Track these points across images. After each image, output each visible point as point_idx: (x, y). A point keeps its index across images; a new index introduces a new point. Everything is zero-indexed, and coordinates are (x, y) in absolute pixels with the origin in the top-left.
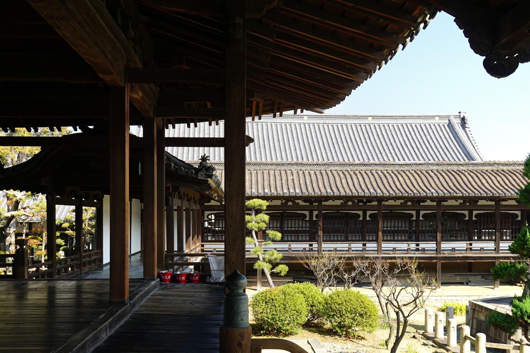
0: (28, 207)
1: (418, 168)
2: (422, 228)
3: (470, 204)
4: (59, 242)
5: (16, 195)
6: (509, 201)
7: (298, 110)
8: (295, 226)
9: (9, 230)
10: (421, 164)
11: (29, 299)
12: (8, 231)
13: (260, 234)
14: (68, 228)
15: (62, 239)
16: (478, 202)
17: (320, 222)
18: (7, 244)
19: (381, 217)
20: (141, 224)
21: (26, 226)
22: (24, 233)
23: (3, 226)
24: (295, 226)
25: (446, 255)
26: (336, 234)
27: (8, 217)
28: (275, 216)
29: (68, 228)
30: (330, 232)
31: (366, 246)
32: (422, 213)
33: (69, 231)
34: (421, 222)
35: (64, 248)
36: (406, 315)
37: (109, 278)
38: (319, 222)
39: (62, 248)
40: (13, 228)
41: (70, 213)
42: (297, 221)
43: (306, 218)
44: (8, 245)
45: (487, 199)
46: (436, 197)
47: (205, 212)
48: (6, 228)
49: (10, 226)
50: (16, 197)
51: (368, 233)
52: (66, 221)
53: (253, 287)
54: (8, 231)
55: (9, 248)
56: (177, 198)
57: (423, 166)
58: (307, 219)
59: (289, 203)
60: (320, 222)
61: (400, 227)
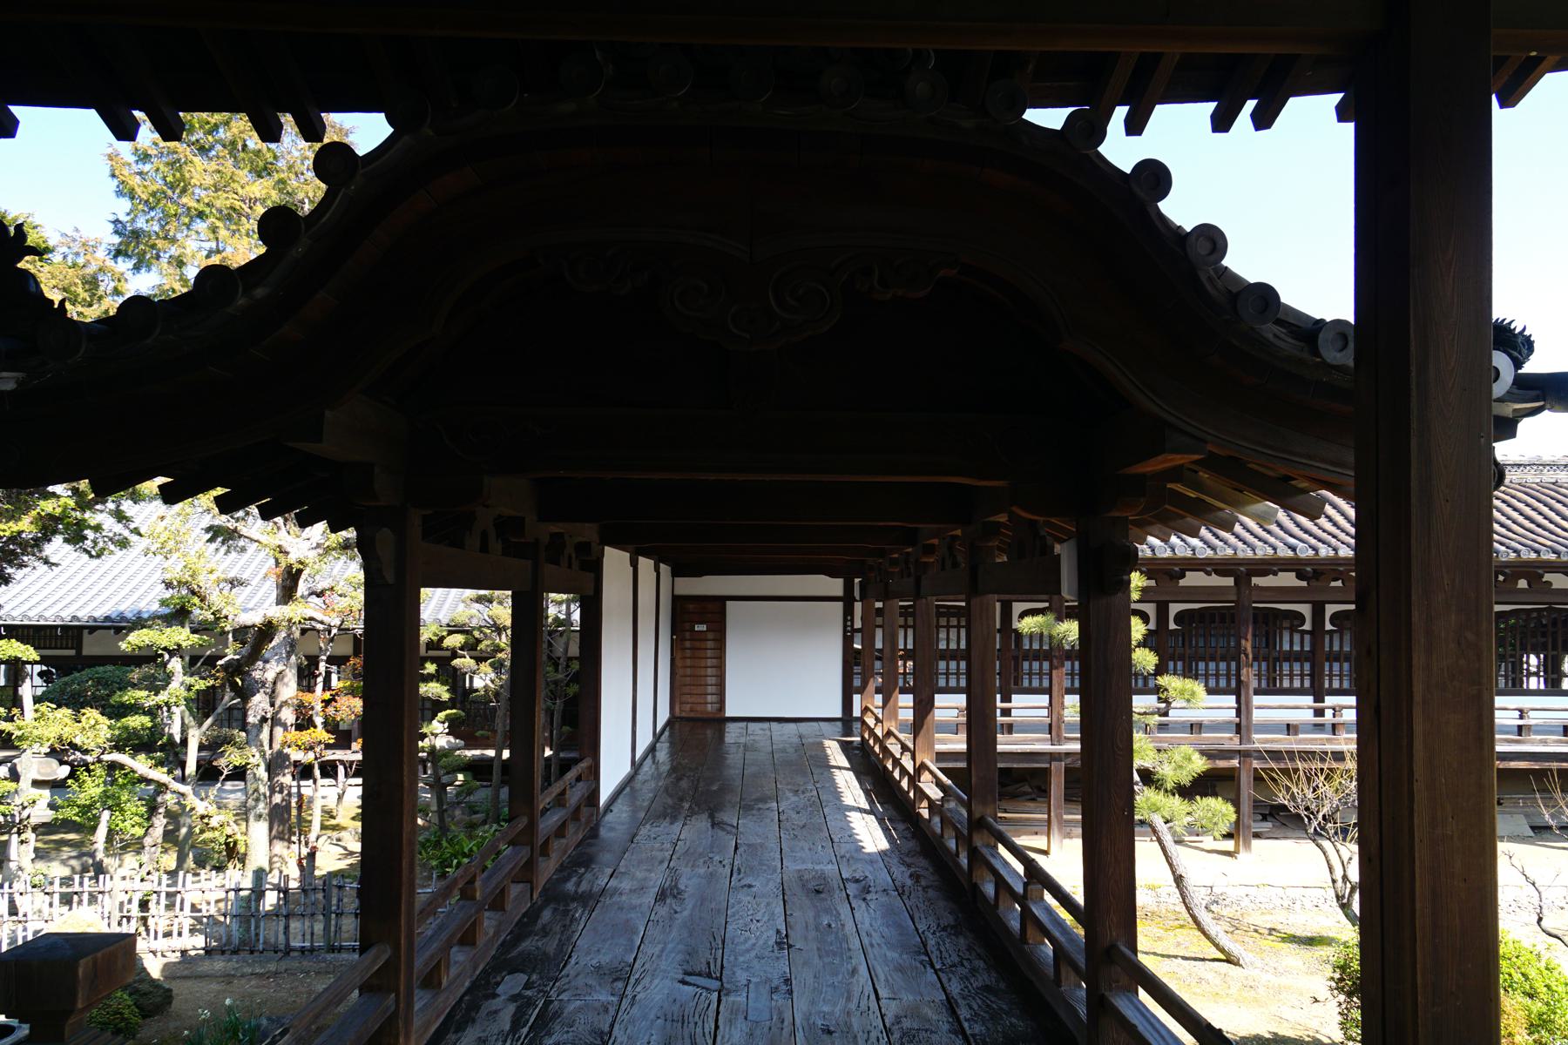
0: (332, 589)
1: (1514, 477)
4: (434, 691)
5: (288, 549)
6: (1280, 573)
9: (264, 670)
10: (1520, 465)
12: (257, 675)
13: (1058, 676)
14: (461, 649)
15: (442, 684)
16: (1183, 576)
17: (1247, 640)
18: (251, 719)
20: (672, 639)
21: (327, 650)
22: (320, 674)
23: (237, 657)
27: (254, 626)
29: (461, 649)
31: (1323, 702)
32: (1174, 609)
33: (463, 659)
35: (447, 716)
38: (1243, 642)
39: (442, 715)
40: (278, 662)
41: (467, 606)
43: (1303, 624)
44: (254, 725)
45: (1209, 569)
46: (1308, 562)
48: (253, 663)
49: (266, 653)
50: (287, 553)
52: (454, 629)
53: (1023, 837)
54: (257, 675)
55: (258, 735)
56: (570, 566)
57: (1526, 471)
58: (1307, 626)
60: (1247, 640)
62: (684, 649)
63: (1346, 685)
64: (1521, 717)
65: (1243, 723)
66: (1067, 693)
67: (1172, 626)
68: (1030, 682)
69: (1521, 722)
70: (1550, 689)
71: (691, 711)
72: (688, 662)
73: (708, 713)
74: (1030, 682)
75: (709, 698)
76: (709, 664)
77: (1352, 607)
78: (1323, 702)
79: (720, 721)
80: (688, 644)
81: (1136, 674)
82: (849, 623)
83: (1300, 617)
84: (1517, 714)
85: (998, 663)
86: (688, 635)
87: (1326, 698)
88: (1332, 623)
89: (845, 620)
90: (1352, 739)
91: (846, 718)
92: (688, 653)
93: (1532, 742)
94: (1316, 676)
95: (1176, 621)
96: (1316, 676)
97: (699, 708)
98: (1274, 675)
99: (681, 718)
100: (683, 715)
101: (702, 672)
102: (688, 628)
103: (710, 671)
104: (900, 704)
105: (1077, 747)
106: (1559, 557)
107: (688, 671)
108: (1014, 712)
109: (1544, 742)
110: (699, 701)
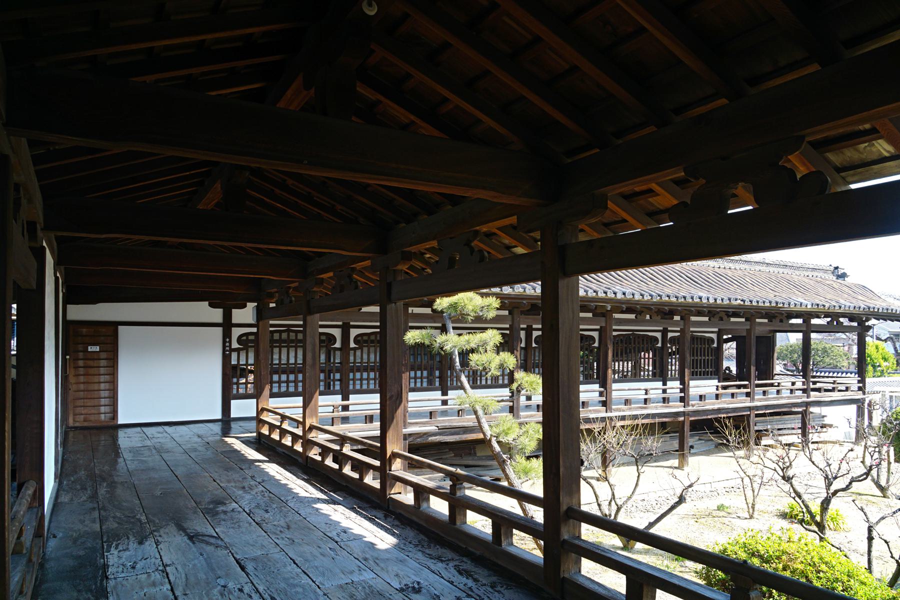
3: (651, 317)
8: (806, 341)
17: (517, 351)
19: (611, 341)
24: (806, 341)
25: (695, 408)
28: (366, 342)
32: (354, 333)
34: (352, 352)
36: (873, 520)
42: (284, 350)
43: (335, 343)
47: (233, 310)
58: (338, 345)
59: (438, 301)
60: (517, 351)
62: (78, 367)
63: (372, 387)
64: (646, 394)
65: (515, 406)
66: (614, 383)
68: (361, 386)
69: (646, 397)
71: (85, 421)
72: (82, 379)
73: (101, 422)
74: (361, 386)
75: (103, 409)
76: (102, 380)
77: (302, 329)
78: (348, 400)
79: (113, 428)
80: (81, 363)
81: (539, 374)
82: (227, 344)
84: (644, 392)
85: (595, 363)
86: (81, 355)
87: (449, 392)
89: (224, 342)
91: (224, 419)
92: (82, 371)
93: (652, 408)
94: (344, 381)
95: (356, 341)
96: (344, 381)
97: (92, 418)
98: (329, 381)
99: (76, 428)
100: (77, 424)
101: (96, 387)
102: (81, 349)
103: (102, 386)
104: (320, 404)
106: (678, 299)
107: (82, 387)
108: (351, 408)
109: (656, 408)
110: (93, 411)
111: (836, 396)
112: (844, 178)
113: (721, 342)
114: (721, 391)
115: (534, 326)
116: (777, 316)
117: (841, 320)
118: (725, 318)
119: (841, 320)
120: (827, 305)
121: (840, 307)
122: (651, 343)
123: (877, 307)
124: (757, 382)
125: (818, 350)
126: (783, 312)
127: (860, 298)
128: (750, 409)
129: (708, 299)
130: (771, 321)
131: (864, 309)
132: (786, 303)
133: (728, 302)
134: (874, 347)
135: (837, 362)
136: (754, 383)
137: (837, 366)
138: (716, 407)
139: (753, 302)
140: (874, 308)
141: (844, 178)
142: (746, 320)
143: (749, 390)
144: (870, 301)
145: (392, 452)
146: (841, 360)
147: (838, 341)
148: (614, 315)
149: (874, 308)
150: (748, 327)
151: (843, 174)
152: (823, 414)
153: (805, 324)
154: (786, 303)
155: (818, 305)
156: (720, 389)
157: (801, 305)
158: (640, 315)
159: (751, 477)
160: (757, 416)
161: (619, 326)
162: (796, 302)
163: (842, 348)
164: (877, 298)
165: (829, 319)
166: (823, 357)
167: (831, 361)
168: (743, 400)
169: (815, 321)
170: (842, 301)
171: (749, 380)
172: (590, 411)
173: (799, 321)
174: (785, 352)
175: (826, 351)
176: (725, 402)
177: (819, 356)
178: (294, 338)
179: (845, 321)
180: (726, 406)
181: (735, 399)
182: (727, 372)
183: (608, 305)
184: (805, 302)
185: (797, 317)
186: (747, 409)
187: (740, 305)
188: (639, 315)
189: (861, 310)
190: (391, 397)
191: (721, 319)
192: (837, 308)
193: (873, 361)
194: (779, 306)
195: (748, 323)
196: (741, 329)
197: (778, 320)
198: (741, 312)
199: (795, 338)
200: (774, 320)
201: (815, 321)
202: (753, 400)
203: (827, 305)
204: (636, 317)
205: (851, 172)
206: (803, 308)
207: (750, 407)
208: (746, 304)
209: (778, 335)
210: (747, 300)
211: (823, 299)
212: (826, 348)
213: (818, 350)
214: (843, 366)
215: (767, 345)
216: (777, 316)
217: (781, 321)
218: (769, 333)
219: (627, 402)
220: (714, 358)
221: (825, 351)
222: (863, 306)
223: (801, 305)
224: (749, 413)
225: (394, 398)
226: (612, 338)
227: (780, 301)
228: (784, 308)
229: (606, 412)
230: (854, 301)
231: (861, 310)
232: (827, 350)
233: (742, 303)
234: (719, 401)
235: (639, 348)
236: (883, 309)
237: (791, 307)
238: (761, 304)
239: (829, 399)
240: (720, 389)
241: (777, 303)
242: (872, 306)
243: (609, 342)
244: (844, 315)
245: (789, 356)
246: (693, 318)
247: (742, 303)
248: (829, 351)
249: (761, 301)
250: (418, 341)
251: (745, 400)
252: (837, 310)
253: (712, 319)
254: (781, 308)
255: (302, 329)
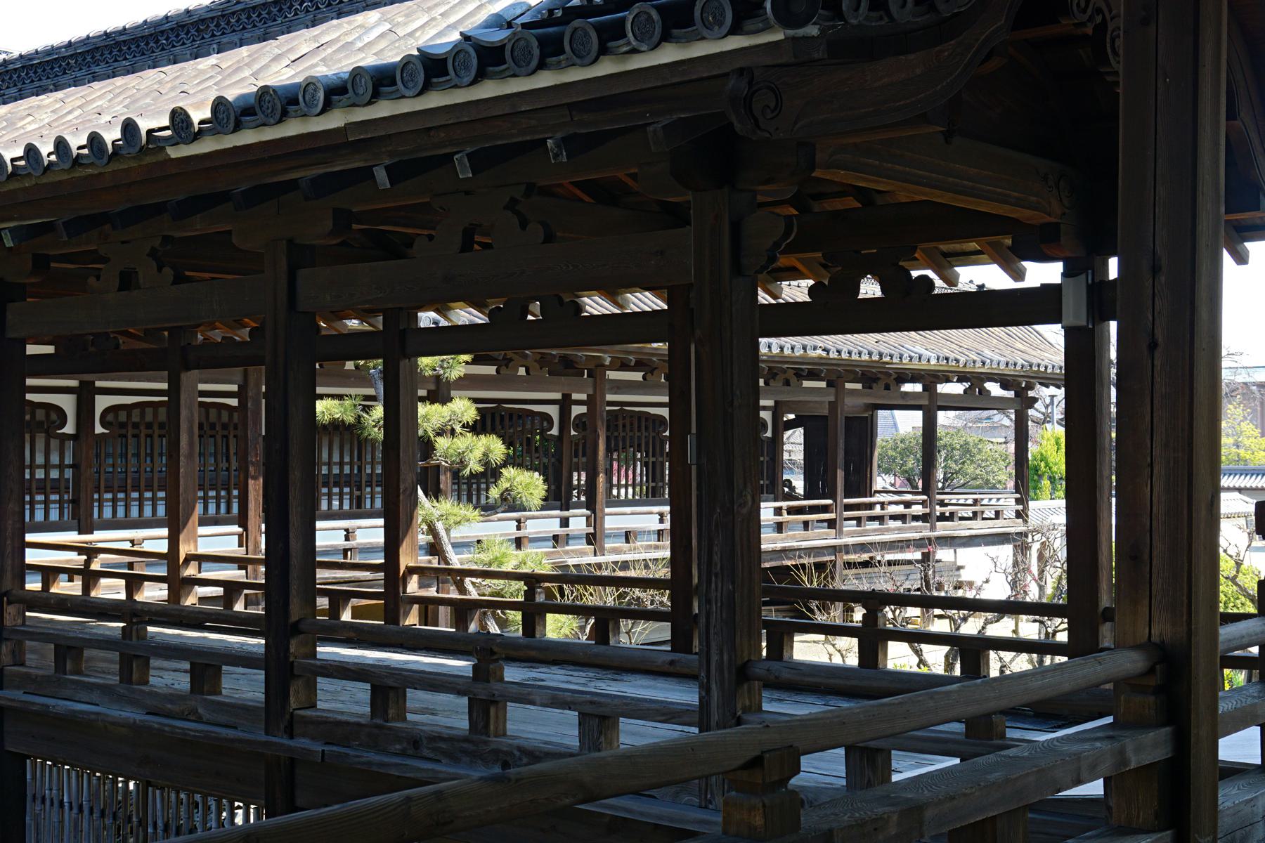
2: (47, 474)
3: (527, 372)
6: (1051, 387)
7: (1116, 276)
8: (930, 425)
11: (1136, 647)
24: (930, 425)
26: (109, 496)
30: (156, 485)
32: (102, 403)
37: (670, 638)
51: (98, 490)
58: (69, 429)
61: (54, 466)
67: (99, 429)
70: (355, 510)
77: (166, 399)
83: (547, 418)
88: (103, 425)
90: (1233, 473)
105: (263, 582)
106: (828, 354)
111: (979, 527)
112: (949, 262)
113: (781, 427)
114: (785, 517)
115: (575, 396)
116: (879, 379)
117: (989, 386)
118: (793, 380)
119: (989, 386)
120: (962, 360)
121: (984, 363)
122: (654, 431)
123: (1043, 363)
124: (846, 501)
125: (953, 449)
126: (891, 371)
127: (1019, 346)
128: (834, 549)
129: (769, 347)
130: (871, 388)
131: (1023, 366)
132: (896, 355)
133: (802, 352)
134: (1053, 441)
135: (987, 473)
136: (842, 501)
137: (988, 480)
138: (779, 546)
139: (843, 353)
140: (1039, 366)
141: (949, 262)
142: (828, 386)
143: (832, 516)
144: (1034, 353)
145: (407, 567)
146: (996, 469)
147: (996, 432)
148: (608, 372)
149: (1039, 366)
150: (832, 399)
151: (948, 259)
152: (959, 564)
153: (926, 393)
154: (896, 355)
155: (947, 359)
156: (785, 512)
157: (920, 358)
158: (774, 380)
159: (844, 653)
160: (849, 565)
161: (615, 393)
162: (913, 354)
163: (1004, 445)
164: (1047, 347)
165: (967, 385)
166: (963, 463)
167: (978, 472)
168: (823, 533)
169: (943, 388)
170: (987, 353)
171: (832, 496)
172: (567, 553)
173: (918, 387)
174: (890, 453)
175: (968, 451)
176: (793, 538)
177: (955, 461)
178: (43, 418)
179: (994, 389)
180: (795, 544)
181: (810, 532)
182: (786, 489)
183: (606, 356)
184: (926, 353)
185: (913, 380)
186: (830, 550)
187: (821, 358)
188: (649, 375)
189: (1018, 368)
190: (405, 490)
191: (787, 383)
192: (979, 364)
193: (1050, 469)
194: (884, 360)
195: (832, 390)
196: (816, 402)
197: (881, 384)
198: (822, 371)
199: (908, 422)
200: (874, 385)
201: (943, 388)
202: (840, 534)
203: (962, 360)
204: (644, 377)
205: (955, 258)
206: (923, 365)
207: (834, 547)
208: (831, 356)
209: (882, 414)
210: (833, 349)
211: (957, 348)
212: (967, 443)
213: (953, 449)
214: (1000, 482)
215: (862, 431)
216: (879, 379)
217: (887, 387)
218: (866, 411)
219: (628, 536)
220: (767, 459)
221: (965, 448)
222: (1020, 362)
223: (920, 358)
224: (833, 558)
225: (408, 492)
226: (605, 414)
227: (886, 351)
228: (892, 363)
229: (595, 555)
230: (1007, 353)
231: (1018, 368)
232: (971, 448)
233: (824, 354)
234: (783, 535)
235: (631, 438)
236: (1053, 367)
237: (904, 361)
238: (855, 357)
239: (967, 533)
240: (785, 512)
241: (881, 355)
242: (1035, 361)
243: (599, 423)
244: (991, 377)
245: (898, 460)
246: (612, 375)
247: (824, 354)
248: (975, 451)
249: (855, 351)
250: (337, 416)
251: (827, 534)
252: (979, 368)
253: (772, 382)
254: (887, 363)
255: (166, 399)
